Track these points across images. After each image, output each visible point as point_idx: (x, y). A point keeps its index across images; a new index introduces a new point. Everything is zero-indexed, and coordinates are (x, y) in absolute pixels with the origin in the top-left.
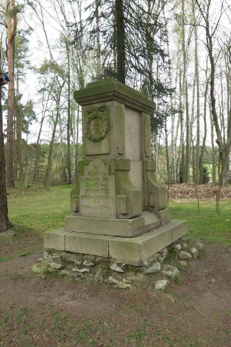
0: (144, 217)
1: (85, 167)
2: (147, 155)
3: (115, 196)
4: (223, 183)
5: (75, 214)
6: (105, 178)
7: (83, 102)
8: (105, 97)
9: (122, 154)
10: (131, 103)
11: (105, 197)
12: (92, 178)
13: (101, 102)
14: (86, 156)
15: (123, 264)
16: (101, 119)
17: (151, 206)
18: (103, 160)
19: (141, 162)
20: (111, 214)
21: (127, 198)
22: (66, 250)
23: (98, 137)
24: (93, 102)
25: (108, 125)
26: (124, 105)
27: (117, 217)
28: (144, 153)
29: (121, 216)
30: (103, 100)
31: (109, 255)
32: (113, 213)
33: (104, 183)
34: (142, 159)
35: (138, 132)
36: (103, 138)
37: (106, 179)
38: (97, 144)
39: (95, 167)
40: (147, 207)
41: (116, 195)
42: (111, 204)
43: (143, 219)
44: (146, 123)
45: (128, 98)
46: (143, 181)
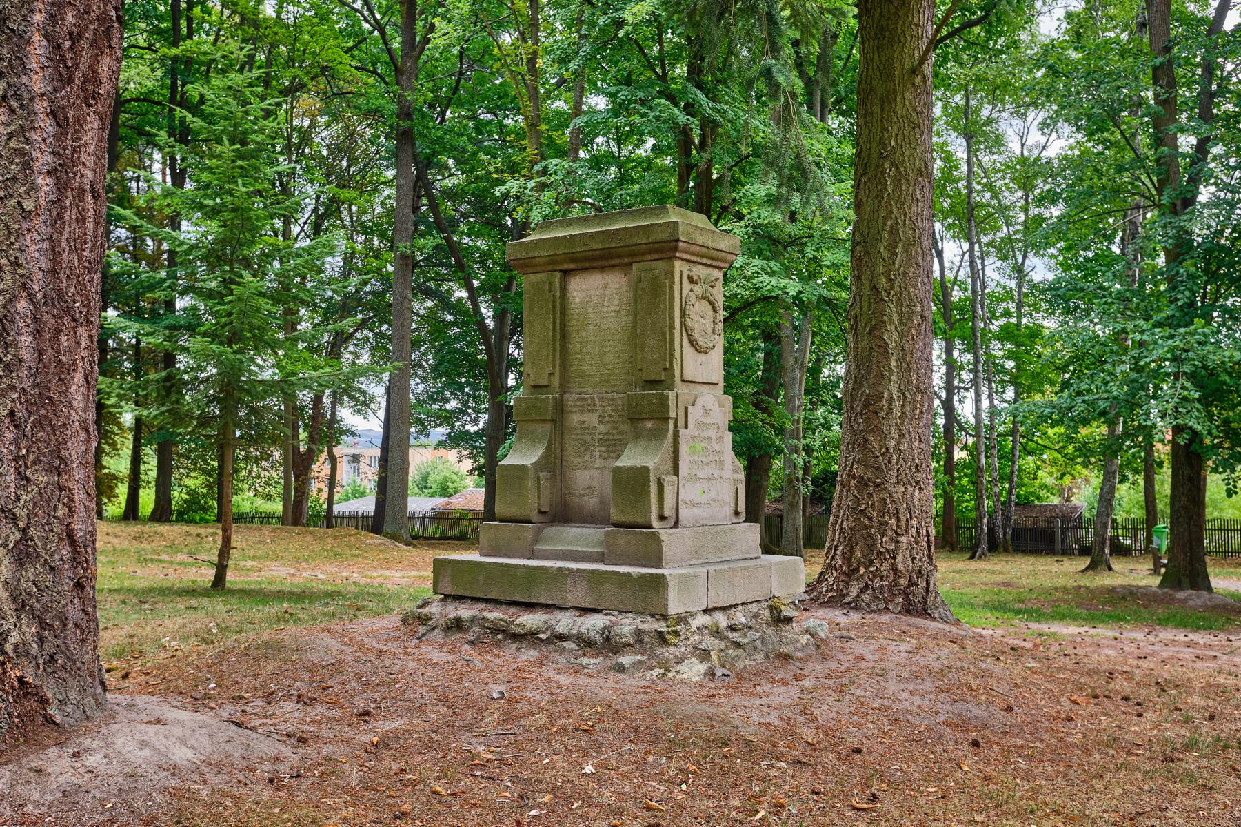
8: (717, 259)
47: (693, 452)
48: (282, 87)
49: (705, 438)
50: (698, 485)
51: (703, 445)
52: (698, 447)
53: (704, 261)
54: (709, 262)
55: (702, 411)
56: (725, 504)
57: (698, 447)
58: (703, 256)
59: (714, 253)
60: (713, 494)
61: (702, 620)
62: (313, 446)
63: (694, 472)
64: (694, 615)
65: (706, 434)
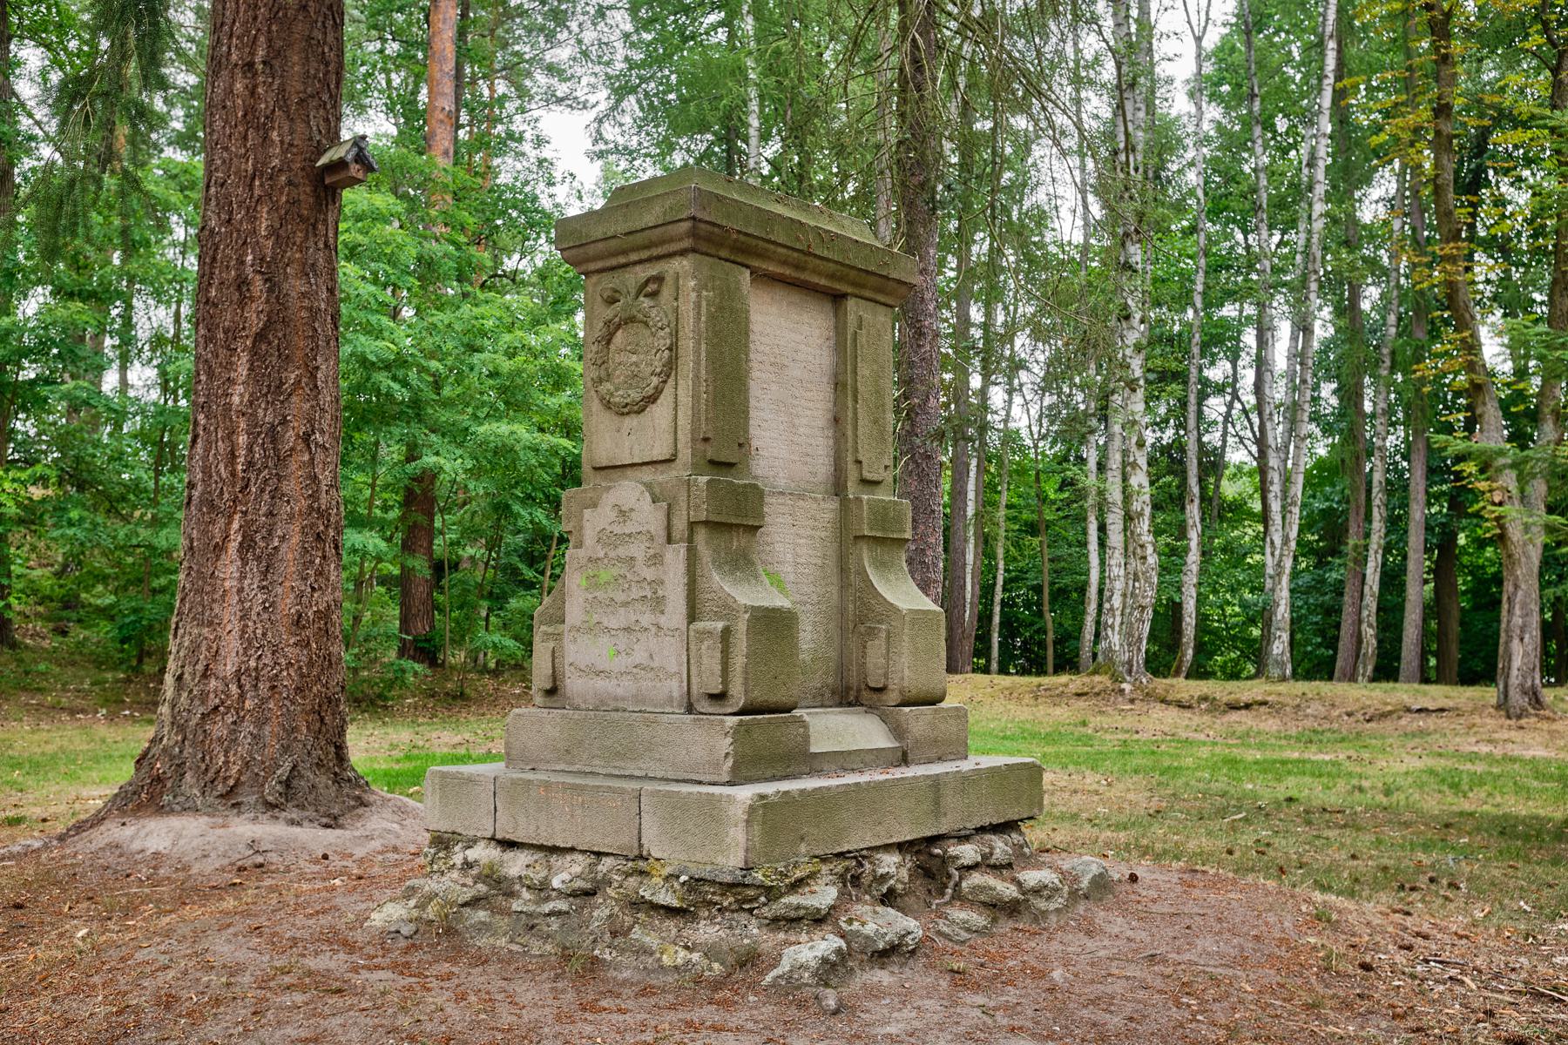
0: (806, 718)
1: (587, 513)
2: (868, 475)
3: (684, 628)
4: (1514, 672)
5: (549, 701)
6: (655, 556)
7: (588, 260)
8: (662, 242)
9: (730, 465)
10: (785, 263)
11: (654, 629)
12: (612, 554)
13: (649, 260)
14: (595, 469)
15: (683, 878)
16: (646, 324)
17: (872, 685)
18: (649, 486)
19: (833, 504)
20: (670, 699)
21: (727, 632)
22: (498, 836)
23: (635, 395)
24: (634, 257)
25: (670, 349)
26: (748, 273)
27: (690, 709)
28: (851, 467)
29: (704, 706)
30: (655, 252)
31: (641, 846)
32: (676, 694)
33: (649, 574)
34: (838, 487)
35: (825, 380)
36: (652, 399)
37: (656, 560)
38: (631, 422)
39: (622, 513)
40: (859, 691)
41: (689, 623)
42: (670, 655)
43: (805, 725)
44: (862, 340)
45: (761, 243)
46: (844, 586)
47: (594, 583)
48: (512, 92)
49: (619, 559)
50: (605, 639)
51: (615, 571)
52: (604, 576)
53: (634, 257)
54: (645, 254)
55: (613, 515)
56: (670, 676)
57: (604, 576)
58: (624, 252)
59: (639, 239)
60: (639, 656)
61: (483, 853)
62: (1362, 542)
63: (596, 618)
64: (471, 843)
65: (622, 552)
